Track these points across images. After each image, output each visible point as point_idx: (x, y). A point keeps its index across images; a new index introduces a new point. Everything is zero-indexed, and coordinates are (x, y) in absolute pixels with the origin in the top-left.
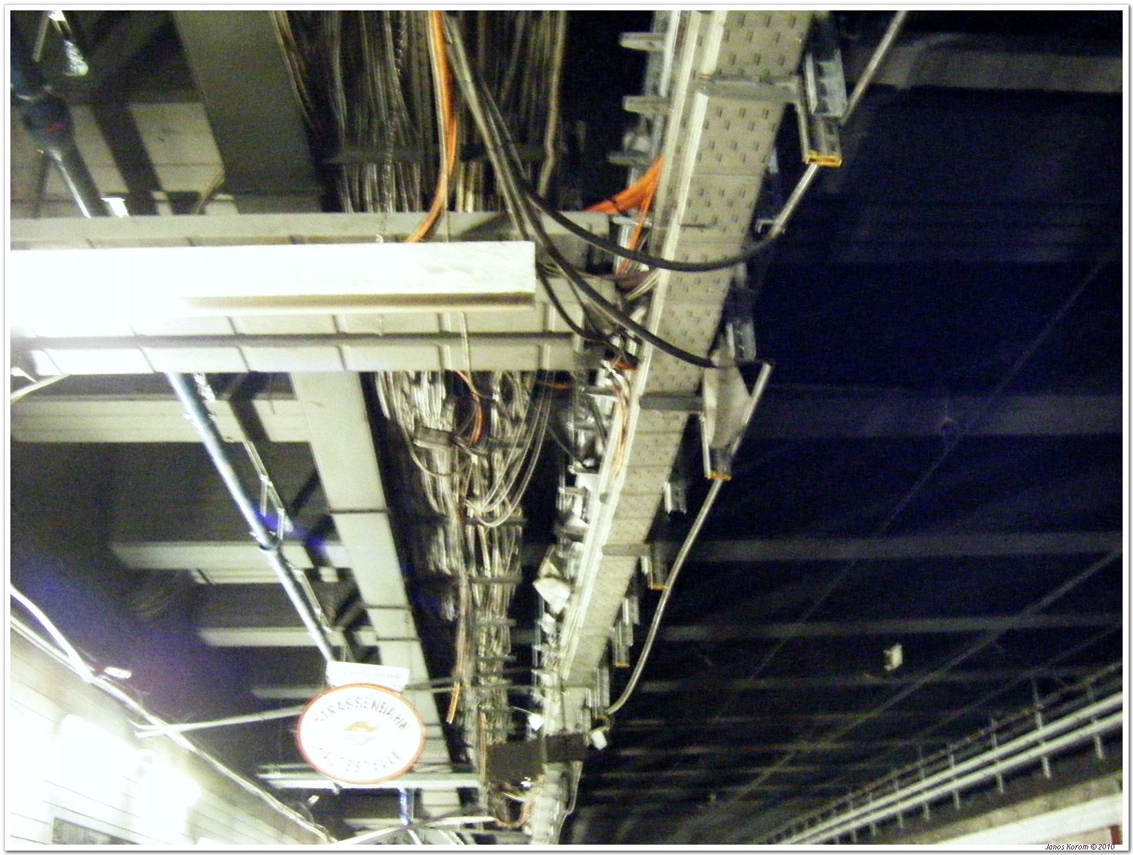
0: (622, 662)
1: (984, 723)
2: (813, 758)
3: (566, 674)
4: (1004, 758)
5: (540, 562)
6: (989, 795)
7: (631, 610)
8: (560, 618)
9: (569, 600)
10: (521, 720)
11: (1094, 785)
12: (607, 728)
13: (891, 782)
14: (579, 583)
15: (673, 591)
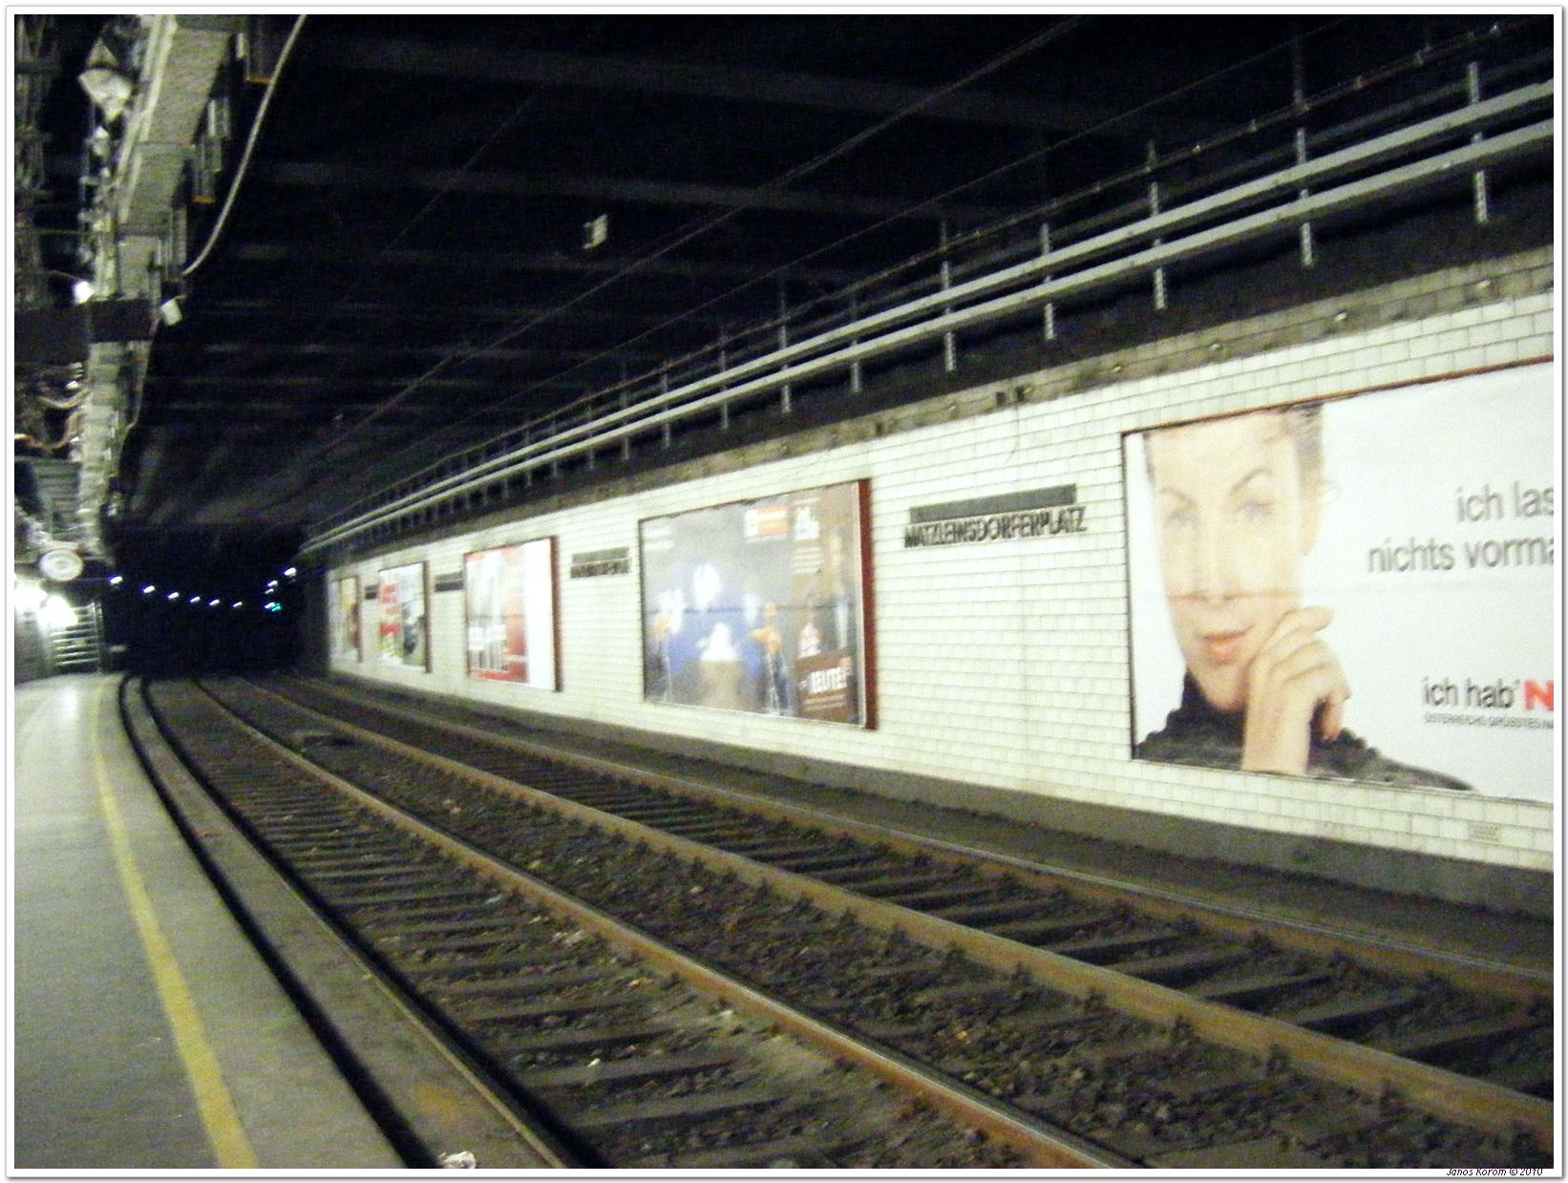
0: (205, 198)
1: (712, 336)
2: (476, 368)
3: (124, 215)
4: (733, 384)
5: (89, 48)
6: (708, 431)
7: (219, 118)
8: (117, 129)
9: (129, 104)
10: (65, 291)
11: (845, 426)
12: (182, 297)
13: (581, 409)
14: (144, 76)
15: (278, 86)
